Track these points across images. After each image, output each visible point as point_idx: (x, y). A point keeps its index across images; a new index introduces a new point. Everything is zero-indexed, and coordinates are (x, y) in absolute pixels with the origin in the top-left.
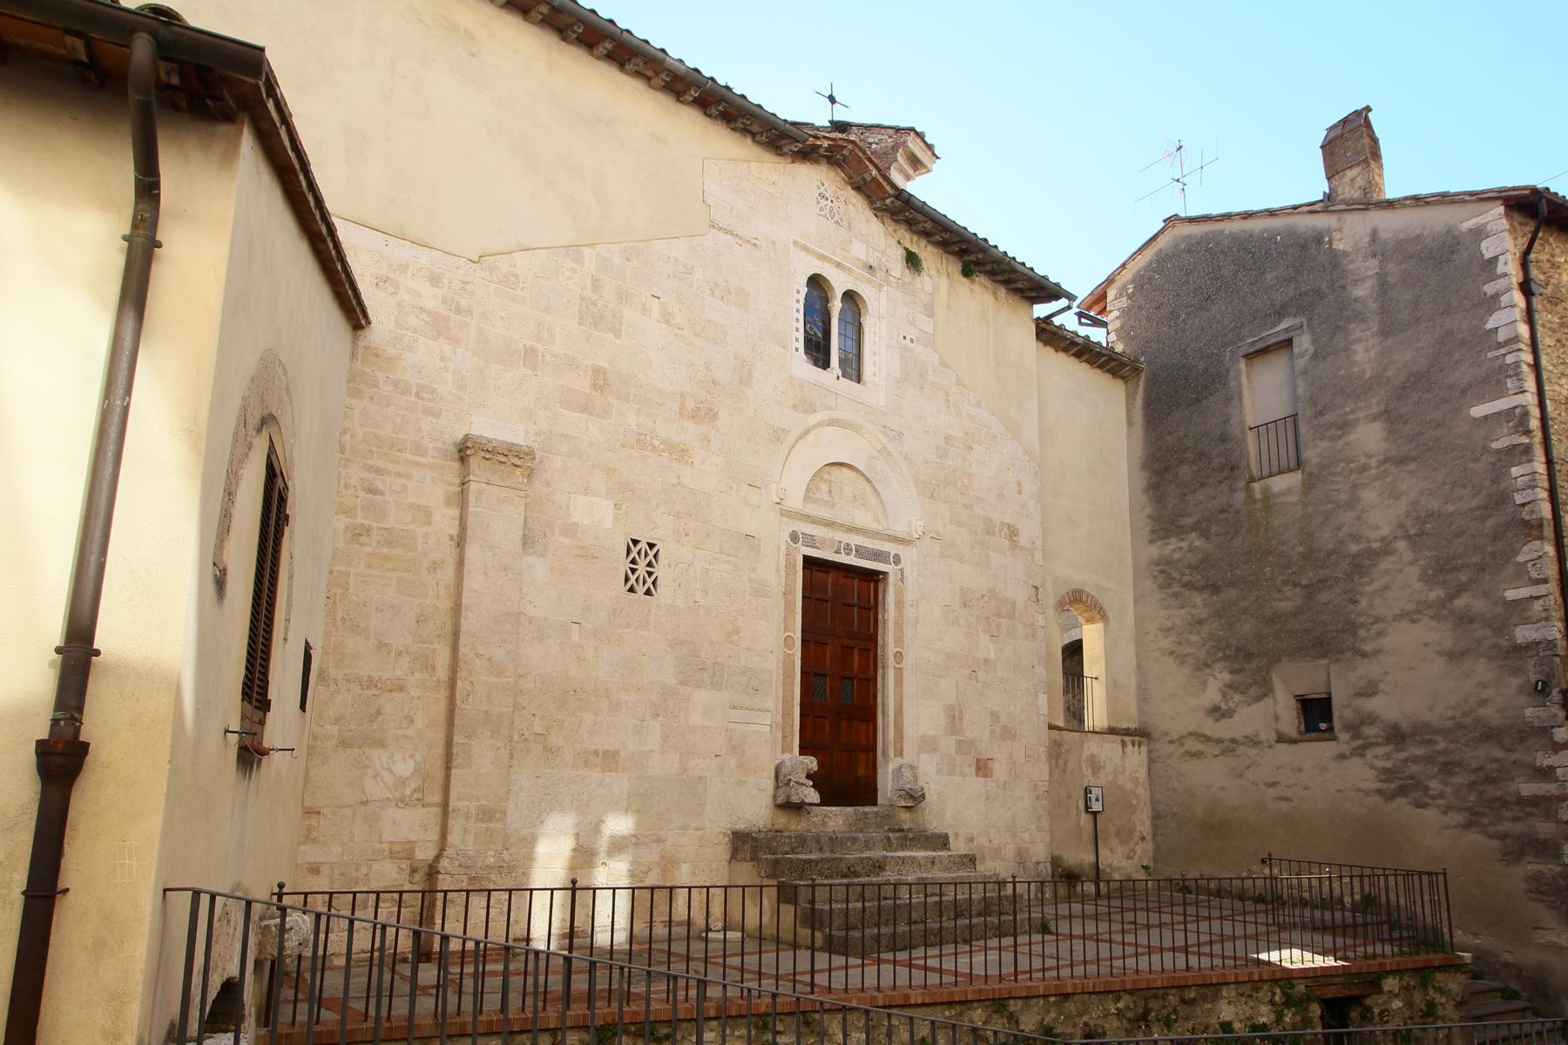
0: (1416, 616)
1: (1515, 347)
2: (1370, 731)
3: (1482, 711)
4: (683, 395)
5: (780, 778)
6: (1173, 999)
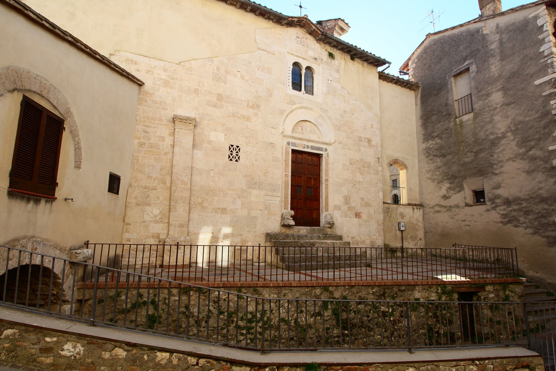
0: (515, 159)
1: (551, 56)
2: (498, 201)
3: (540, 192)
4: (248, 101)
5: (283, 218)
6: (395, 289)
